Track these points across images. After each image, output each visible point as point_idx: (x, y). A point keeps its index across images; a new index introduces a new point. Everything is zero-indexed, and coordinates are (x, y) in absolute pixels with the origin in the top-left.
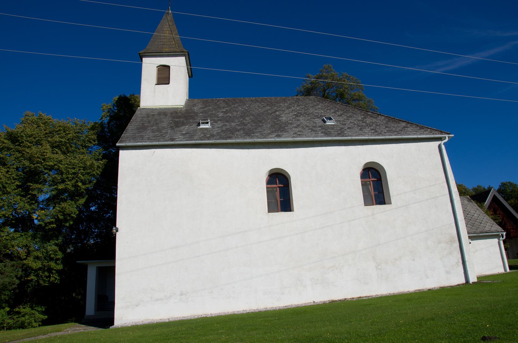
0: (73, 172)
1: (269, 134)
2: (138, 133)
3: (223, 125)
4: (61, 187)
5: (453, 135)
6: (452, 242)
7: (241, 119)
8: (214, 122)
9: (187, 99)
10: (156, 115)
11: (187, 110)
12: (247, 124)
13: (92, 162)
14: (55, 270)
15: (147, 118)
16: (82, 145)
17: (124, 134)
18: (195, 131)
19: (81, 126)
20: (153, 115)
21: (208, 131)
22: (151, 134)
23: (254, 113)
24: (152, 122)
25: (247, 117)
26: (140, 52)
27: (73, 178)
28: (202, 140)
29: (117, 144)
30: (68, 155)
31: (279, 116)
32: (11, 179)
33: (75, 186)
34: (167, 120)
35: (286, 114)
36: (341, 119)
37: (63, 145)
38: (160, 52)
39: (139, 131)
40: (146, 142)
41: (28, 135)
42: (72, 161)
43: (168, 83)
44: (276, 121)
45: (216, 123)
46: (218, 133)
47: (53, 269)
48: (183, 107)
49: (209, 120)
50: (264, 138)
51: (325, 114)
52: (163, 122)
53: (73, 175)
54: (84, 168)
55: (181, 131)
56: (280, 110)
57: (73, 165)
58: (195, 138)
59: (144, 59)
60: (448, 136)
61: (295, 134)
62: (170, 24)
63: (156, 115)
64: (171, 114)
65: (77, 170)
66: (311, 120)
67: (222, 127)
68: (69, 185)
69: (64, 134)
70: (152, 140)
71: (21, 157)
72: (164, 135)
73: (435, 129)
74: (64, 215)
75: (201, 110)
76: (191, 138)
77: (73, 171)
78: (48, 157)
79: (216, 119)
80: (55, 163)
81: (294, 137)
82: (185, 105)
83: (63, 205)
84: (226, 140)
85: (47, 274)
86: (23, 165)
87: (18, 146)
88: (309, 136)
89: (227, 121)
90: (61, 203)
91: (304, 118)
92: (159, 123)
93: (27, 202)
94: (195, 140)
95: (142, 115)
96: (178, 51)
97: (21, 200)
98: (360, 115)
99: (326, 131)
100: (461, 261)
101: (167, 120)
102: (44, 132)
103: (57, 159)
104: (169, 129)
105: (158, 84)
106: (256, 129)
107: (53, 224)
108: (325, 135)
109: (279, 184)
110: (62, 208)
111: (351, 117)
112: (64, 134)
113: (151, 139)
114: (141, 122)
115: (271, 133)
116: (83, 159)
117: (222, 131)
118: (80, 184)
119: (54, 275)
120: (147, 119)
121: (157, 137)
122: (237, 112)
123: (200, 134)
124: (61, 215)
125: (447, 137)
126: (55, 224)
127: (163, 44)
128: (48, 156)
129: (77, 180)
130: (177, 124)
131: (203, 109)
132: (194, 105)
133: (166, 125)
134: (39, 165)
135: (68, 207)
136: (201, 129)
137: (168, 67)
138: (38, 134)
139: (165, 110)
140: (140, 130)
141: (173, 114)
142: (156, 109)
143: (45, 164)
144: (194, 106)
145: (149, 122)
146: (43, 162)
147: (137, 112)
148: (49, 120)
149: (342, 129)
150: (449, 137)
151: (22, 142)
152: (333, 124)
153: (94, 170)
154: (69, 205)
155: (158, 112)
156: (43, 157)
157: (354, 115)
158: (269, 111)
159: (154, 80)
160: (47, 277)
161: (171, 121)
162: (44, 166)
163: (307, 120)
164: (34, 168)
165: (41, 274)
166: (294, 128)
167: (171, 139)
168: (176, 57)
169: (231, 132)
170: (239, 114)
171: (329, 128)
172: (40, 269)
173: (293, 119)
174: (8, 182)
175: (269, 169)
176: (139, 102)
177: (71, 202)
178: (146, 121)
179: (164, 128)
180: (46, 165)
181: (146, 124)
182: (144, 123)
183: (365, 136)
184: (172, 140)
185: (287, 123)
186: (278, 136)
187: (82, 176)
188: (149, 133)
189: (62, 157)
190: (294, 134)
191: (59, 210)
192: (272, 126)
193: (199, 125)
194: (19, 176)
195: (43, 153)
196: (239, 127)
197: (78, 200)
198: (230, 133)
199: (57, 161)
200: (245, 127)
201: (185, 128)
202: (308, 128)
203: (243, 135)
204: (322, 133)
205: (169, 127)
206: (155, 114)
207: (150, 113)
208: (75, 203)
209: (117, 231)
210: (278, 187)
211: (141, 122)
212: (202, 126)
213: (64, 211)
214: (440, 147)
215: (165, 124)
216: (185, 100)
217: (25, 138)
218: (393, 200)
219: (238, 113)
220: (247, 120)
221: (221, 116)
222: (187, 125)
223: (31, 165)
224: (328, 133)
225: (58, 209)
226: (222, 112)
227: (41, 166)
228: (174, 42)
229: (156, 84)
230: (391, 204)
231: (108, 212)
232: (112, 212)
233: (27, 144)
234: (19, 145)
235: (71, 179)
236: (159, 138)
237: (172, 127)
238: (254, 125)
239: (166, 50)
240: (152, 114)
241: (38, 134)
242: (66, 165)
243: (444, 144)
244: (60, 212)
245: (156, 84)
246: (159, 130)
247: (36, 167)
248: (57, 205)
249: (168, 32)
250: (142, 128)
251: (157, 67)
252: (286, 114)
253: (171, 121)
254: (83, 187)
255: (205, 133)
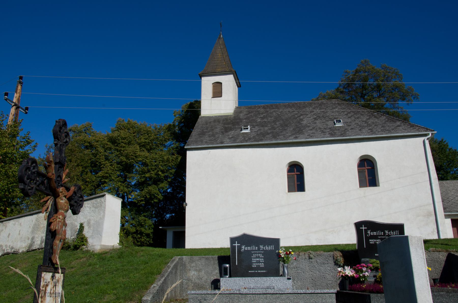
0: (155, 165)
1: (290, 136)
2: (199, 138)
3: (259, 130)
4: (147, 175)
5: (436, 132)
6: (429, 215)
7: (273, 124)
8: (253, 127)
9: (236, 107)
10: (212, 122)
11: (235, 117)
12: (276, 128)
13: (168, 157)
14: (144, 233)
15: (205, 125)
16: (160, 144)
17: (190, 139)
18: (238, 135)
19: (159, 130)
20: (210, 122)
21: (247, 135)
22: (208, 138)
23: (284, 118)
24: (209, 128)
25: (278, 121)
26: (200, 73)
27: (156, 169)
28: (242, 142)
29: (185, 147)
30: (151, 151)
31: (302, 120)
32: (114, 170)
33: (157, 174)
34: (220, 126)
35: (307, 118)
36: (349, 120)
37: (148, 145)
38: (215, 72)
39: (200, 137)
40: (204, 145)
41: (122, 137)
42: (154, 156)
43: (221, 96)
44: (298, 124)
45: (254, 127)
46: (254, 137)
47: (143, 233)
48: (232, 114)
49: (249, 126)
50: (285, 140)
51: (338, 117)
52: (216, 128)
53: (155, 167)
54: (163, 161)
55: (228, 136)
56: (304, 115)
57: (155, 159)
58: (237, 141)
59: (202, 78)
60: (431, 132)
61: (309, 135)
62: (222, 47)
63: (212, 122)
64: (223, 121)
65: (158, 163)
66: (325, 123)
67: (257, 131)
68: (153, 174)
69: (147, 136)
70: (208, 144)
71: (119, 154)
72: (216, 139)
73: (423, 127)
74: (150, 195)
75: (245, 116)
76: (234, 141)
77: (155, 164)
78: (139, 155)
79: (255, 124)
80: (143, 158)
81: (307, 138)
82: (234, 112)
83: (150, 188)
84: (258, 142)
85: (139, 236)
86: (121, 160)
87: (117, 146)
88: (318, 138)
89: (263, 126)
90: (148, 187)
91: (320, 121)
92: (214, 129)
93: (125, 186)
94: (237, 143)
95: (202, 123)
96: (227, 71)
97: (121, 185)
98: (366, 116)
99: (333, 131)
100: (436, 231)
101: (220, 126)
102: (133, 135)
103: (144, 155)
104: (220, 134)
105: (213, 97)
106: (281, 132)
107: (143, 201)
108: (330, 136)
109: (296, 172)
110: (149, 190)
111: (358, 118)
112: (147, 136)
113: (208, 143)
114: (202, 129)
115: (291, 135)
116: (161, 155)
117: (257, 135)
118: (160, 173)
119: (144, 237)
120: (206, 126)
121: (212, 141)
122: (271, 117)
123: (241, 137)
124: (148, 195)
125: (430, 134)
126: (144, 201)
127: (216, 65)
128: (138, 154)
129: (158, 170)
130: (226, 130)
131: (247, 116)
132: (241, 112)
133: (219, 131)
134: (132, 160)
135: (153, 189)
136: (243, 133)
137: (220, 83)
138: (129, 136)
139: (219, 117)
140: (201, 136)
141: (224, 121)
142: (212, 117)
143: (136, 159)
144: (240, 113)
145: (207, 129)
146: (135, 158)
147: (199, 120)
148: (136, 124)
149: (346, 129)
150: (432, 134)
151: (119, 144)
152: (341, 125)
153: (170, 162)
154: (153, 188)
155: (214, 119)
156: (135, 155)
157: (362, 117)
158: (296, 115)
159: (211, 94)
160: (139, 238)
161: (222, 128)
162: (136, 161)
163: (322, 123)
164: (130, 162)
165: (135, 236)
166: (310, 130)
167: (221, 142)
168: (227, 75)
169: (263, 135)
170: (273, 119)
171: (336, 129)
172: (134, 233)
173: (312, 122)
174: (112, 173)
175: (289, 162)
176: (200, 113)
177: (154, 186)
178: (205, 128)
179: (217, 133)
180: (137, 160)
181: (204, 131)
182: (203, 130)
183: (361, 136)
184: (222, 143)
185: (306, 126)
186: (296, 138)
187: (161, 167)
188: (206, 138)
189: (147, 154)
190: (308, 135)
191: (146, 192)
192: (294, 129)
193: (241, 130)
194: (118, 168)
195: (135, 152)
196: (270, 131)
197: (159, 185)
198: (262, 137)
199: (144, 157)
200: (274, 131)
201: (232, 133)
202: (320, 130)
203: (271, 137)
204: (329, 134)
205: (221, 132)
206: (211, 122)
207: (208, 121)
208: (157, 186)
209: (186, 205)
210: (296, 174)
211: (202, 129)
212: (244, 131)
213: (151, 192)
214: (424, 142)
215: (217, 130)
216: (235, 107)
217: (121, 141)
218: (380, 184)
219: (272, 118)
220: (277, 124)
221: (259, 122)
222: (233, 131)
223: (128, 160)
224: (334, 134)
225: (146, 191)
226: (261, 118)
227: (134, 161)
228: (224, 63)
229: (212, 98)
230: (379, 186)
231: (180, 193)
232: (183, 193)
233: (123, 145)
234: (117, 146)
235: (154, 169)
236: (213, 141)
237: (222, 132)
238: (281, 128)
239: (219, 70)
240: (209, 121)
241: (129, 136)
242: (150, 160)
243: (428, 139)
244: (147, 193)
245: (212, 98)
246: (213, 135)
247: (131, 162)
248: (145, 188)
249: (220, 54)
250: (202, 133)
251: (212, 84)
252: (307, 118)
253: (222, 128)
254: (163, 175)
255: (246, 137)
